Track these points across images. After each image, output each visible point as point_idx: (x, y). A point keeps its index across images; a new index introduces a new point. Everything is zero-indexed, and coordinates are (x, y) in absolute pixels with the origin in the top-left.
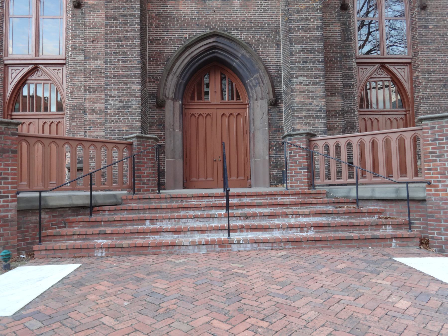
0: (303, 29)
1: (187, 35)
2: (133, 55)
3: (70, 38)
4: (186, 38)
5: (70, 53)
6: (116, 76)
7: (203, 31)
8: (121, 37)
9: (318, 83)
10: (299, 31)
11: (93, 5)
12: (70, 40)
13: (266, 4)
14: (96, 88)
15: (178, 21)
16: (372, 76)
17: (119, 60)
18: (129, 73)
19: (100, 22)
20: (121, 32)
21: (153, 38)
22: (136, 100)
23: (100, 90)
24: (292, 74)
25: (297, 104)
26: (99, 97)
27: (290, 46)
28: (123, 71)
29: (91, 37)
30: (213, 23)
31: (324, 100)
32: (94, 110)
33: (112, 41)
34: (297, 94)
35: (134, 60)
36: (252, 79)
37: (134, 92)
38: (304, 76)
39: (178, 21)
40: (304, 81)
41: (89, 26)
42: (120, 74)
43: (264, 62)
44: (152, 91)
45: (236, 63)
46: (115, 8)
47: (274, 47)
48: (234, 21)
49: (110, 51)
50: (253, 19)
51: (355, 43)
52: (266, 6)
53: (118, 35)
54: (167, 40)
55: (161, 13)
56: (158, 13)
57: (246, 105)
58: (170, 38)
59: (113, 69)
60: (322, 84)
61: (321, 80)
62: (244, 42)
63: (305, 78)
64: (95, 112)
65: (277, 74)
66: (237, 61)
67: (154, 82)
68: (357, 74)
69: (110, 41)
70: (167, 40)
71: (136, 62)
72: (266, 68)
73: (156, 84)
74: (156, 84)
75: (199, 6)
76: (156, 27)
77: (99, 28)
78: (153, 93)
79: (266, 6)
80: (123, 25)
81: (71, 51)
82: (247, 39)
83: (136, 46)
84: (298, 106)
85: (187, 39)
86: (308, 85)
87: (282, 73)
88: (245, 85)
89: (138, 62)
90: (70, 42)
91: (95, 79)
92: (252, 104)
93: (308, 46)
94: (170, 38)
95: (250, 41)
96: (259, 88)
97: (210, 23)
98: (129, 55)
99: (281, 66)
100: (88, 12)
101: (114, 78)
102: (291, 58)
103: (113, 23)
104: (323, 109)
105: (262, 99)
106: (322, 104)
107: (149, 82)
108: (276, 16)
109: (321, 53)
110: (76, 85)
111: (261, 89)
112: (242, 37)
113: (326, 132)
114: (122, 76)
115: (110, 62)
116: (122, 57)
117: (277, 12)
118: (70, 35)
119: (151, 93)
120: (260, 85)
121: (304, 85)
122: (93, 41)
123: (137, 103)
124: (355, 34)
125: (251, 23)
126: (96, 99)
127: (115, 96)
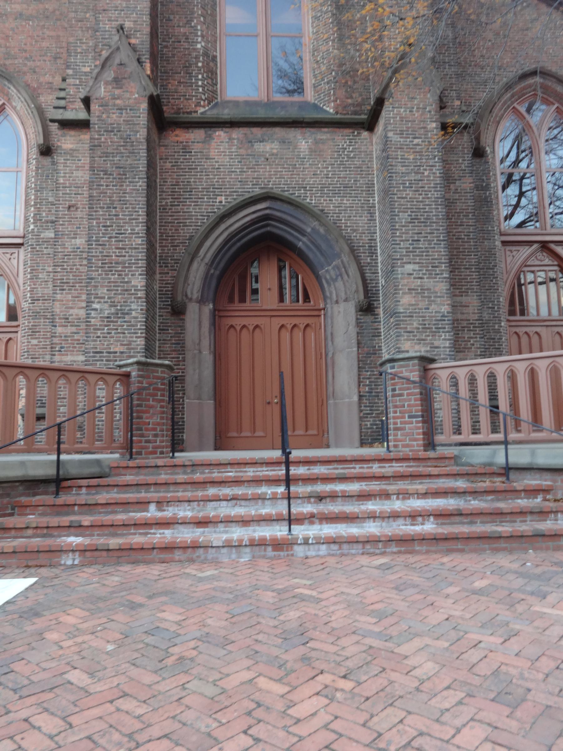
2: (134, 230)
3: (33, 203)
4: (221, 202)
5: (32, 227)
6: (106, 263)
7: (249, 192)
8: (114, 201)
11: (71, 150)
12: (31, 206)
16: (528, 263)
17: (110, 237)
18: (127, 258)
19: (82, 177)
20: (115, 193)
21: (167, 203)
22: (138, 302)
23: (79, 286)
24: (395, 259)
25: (404, 309)
28: (117, 256)
29: (66, 201)
31: (449, 302)
32: (67, 319)
33: (100, 208)
35: (136, 237)
36: (330, 268)
37: (135, 290)
38: (414, 263)
40: (414, 270)
41: (63, 184)
42: (112, 260)
43: (350, 243)
45: (304, 243)
46: (107, 154)
48: (299, 175)
49: (97, 223)
50: (330, 171)
51: (498, 210)
53: (110, 197)
54: (191, 205)
55: (181, 162)
56: (175, 162)
57: (320, 310)
59: (101, 252)
60: (444, 275)
62: (315, 209)
63: (416, 267)
64: (69, 322)
66: (304, 239)
68: (503, 260)
69: (97, 208)
71: (139, 241)
72: (353, 251)
75: (243, 151)
76: (172, 185)
77: (79, 187)
80: (118, 182)
81: (33, 223)
82: (321, 203)
83: (139, 215)
84: (406, 313)
85: (223, 203)
86: (421, 278)
88: (318, 278)
89: (142, 241)
90: (32, 209)
92: (329, 309)
95: (326, 207)
96: (342, 283)
98: (127, 230)
100: (63, 161)
102: (392, 233)
104: (446, 317)
105: (346, 300)
106: (445, 309)
107: (160, 273)
109: (442, 226)
111: (344, 283)
114: (117, 263)
115: (96, 241)
116: (116, 234)
120: (342, 278)
121: (415, 278)
122: (69, 207)
123: (139, 308)
124: (497, 195)
126: (71, 301)
127: (103, 295)
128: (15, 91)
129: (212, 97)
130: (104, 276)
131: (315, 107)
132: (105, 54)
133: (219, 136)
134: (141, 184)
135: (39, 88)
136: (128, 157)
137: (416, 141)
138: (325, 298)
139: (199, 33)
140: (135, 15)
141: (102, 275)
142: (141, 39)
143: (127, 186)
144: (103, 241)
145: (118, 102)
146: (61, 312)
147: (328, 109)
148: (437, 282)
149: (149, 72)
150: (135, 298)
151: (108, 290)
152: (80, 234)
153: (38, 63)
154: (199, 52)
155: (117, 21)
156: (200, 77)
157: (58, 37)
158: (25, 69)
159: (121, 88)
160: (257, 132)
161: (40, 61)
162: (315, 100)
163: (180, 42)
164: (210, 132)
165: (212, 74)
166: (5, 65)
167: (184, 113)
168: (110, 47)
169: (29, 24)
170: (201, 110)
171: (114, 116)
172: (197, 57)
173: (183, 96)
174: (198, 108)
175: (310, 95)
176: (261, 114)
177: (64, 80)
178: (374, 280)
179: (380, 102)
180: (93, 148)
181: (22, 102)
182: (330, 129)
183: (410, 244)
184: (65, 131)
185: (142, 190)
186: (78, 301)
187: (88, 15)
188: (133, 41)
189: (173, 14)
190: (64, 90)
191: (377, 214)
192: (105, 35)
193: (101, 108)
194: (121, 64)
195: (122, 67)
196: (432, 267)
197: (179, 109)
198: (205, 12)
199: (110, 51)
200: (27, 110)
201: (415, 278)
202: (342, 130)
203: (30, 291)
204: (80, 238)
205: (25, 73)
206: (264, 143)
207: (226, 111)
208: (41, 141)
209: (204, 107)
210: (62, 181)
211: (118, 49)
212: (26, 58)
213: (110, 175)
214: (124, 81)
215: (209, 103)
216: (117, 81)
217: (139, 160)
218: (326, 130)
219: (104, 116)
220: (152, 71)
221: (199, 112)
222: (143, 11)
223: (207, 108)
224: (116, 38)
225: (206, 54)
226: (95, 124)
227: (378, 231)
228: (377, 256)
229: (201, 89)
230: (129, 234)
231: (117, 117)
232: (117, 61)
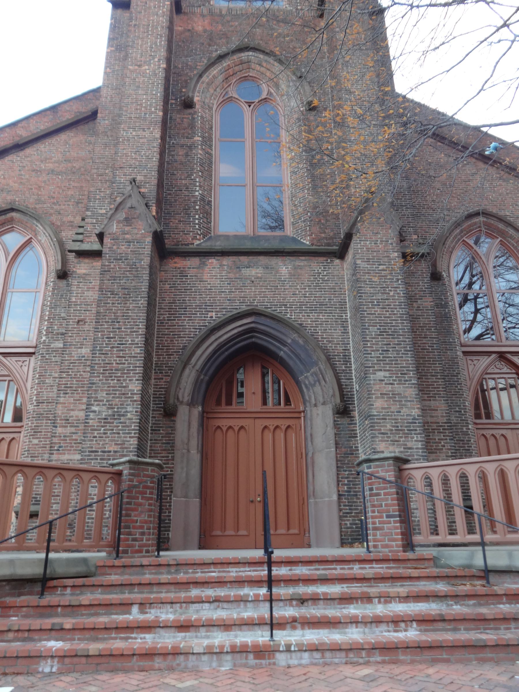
0: (379, 305)
1: (214, 313)
2: (134, 341)
3: (47, 318)
5: (44, 338)
6: (107, 370)
7: (237, 309)
8: (118, 316)
9: (407, 381)
10: (374, 308)
11: (84, 274)
12: (45, 321)
14: (76, 387)
16: (489, 371)
17: (113, 347)
18: (126, 365)
19: (91, 296)
21: (164, 318)
22: (133, 405)
23: (81, 390)
24: (367, 367)
25: (377, 412)
26: (79, 400)
27: (363, 329)
28: (117, 364)
29: (76, 316)
30: (251, 297)
31: (419, 406)
32: (68, 420)
33: (106, 322)
34: (376, 398)
35: (135, 347)
36: (309, 374)
37: (131, 394)
38: (385, 370)
40: (385, 377)
41: (75, 302)
42: (113, 367)
44: (158, 391)
45: (284, 352)
46: (114, 278)
47: (339, 330)
50: (307, 292)
51: (457, 324)
54: (185, 320)
59: (103, 360)
60: (413, 382)
61: (411, 377)
62: (295, 323)
63: (387, 374)
64: (69, 423)
65: (345, 367)
66: (285, 349)
67: (162, 379)
70: (185, 320)
71: (138, 350)
72: (329, 359)
73: (165, 382)
74: (165, 382)
75: (231, 275)
77: (88, 305)
78: (160, 394)
81: (46, 335)
83: (139, 328)
84: (379, 415)
85: (214, 318)
86: (392, 384)
87: (353, 365)
88: (298, 383)
89: (141, 350)
90: (46, 323)
91: (75, 375)
92: (309, 412)
93: (389, 329)
96: (319, 388)
98: (128, 341)
99: (350, 355)
101: (103, 374)
103: (110, 297)
104: (417, 419)
105: (324, 404)
106: (416, 412)
107: (155, 379)
109: (408, 338)
110: (46, 383)
112: (292, 316)
114: (116, 370)
115: (99, 350)
116: (118, 344)
118: (47, 313)
119: (156, 394)
120: (320, 383)
121: (386, 384)
122: (79, 321)
123: (134, 410)
126: (73, 403)
127: (102, 399)
129: (206, 232)
130: (104, 381)
131: (294, 240)
132: (119, 200)
133: (212, 263)
134: (143, 302)
135: (61, 225)
136: (133, 280)
137: (381, 267)
138: (304, 402)
139: (198, 184)
141: (102, 380)
142: (150, 188)
143: (130, 304)
144: (106, 350)
145: (127, 236)
146: (63, 413)
147: (305, 241)
148: (407, 387)
149: (154, 214)
150: (131, 401)
151: (107, 394)
152: (86, 345)
153: (63, 207)
156: (197, 217)
157: (82, 187)
158: (52, 211)
159: (131, 226)
160: (244, 259)
164: (204, 260)
165: (207, 215)
166: (35, 208)
167: (182, 245)
169: (58, 178)
170: (198, 242)
171: (123, 247)
172: (195, 202)
174: (194, 241)
175: (289, 231)
176: (248, 245)
177: (83, 219)
178: (349, 385)
179: (349, 237)
180: (103, 273)
181: (46, 236)
182: (307, 258)
183: (380, 354)
184: (81, 259)
185: (143, 307)
186: (79, 403)
187: (107, 171)
188: (142, 190)
190: (83, 227)
191: (350, 328)
194: (132, 208)
195: (133, 210)
196: (401, 374)
197: (178, 242)
198: (203, 169)
199: (123, 197)
201: (386, 384)
202: (317, 258)
203: (36, 395)
204: (86, 348)
205: (51, 215)
207: (218, 243)
208: (59, 267)
209: (199, 240)
210: (74, 300)
211: (130, 196)
212: (54, 203)
213: (116, 294)
214: (133, 220)
216: (128, 221)
217: (142, 282)
218: (303, 258)
220: (157, 212)
223: (202, 241)
224: (129, 188)
225: (202, 199)
226: (107, 254)
227: (351, 342)
228: (351, 364)
229: (197, 226)
230: (130, 344)
232: (129, 205)
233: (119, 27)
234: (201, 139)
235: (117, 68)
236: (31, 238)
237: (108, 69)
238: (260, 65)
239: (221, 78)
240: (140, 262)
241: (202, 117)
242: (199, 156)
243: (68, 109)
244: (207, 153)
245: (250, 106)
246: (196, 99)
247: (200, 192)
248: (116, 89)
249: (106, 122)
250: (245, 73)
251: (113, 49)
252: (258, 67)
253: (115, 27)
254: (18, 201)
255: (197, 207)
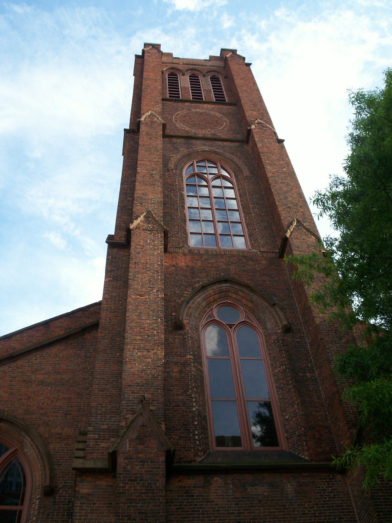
11: (88, 494)
13: (330, 489)
15: (210, 517)
19: (96, 519)
39: (210, 517)
48: (290, 514)
52: (330, 492)
55: (185, 505)
56: (180, 505)
58: (194, 511)
79: (330, 492)
94: (194, 511)
97: (257, 519)
100: (79, 504)
108: (348, 506)
113: (88, 447)
117: (347, 500)
125: (315, 517)
128: (29, 440)
132: (130, 417)
133: (217, 481)
139: (194, 400)
140: (152, 389)
145: (141, 455)
147: (303, 457)
154: (195, 414)
155: (139, 393)
156: (196, 432)
159: (143, 445)
161: (53, 416)
162: (290, 449)
163: (179, 406)
168: (134, 412)
169: (48, 389)
170: (200, 459)
171: (138, 467)
172: (193, 418)
173: (184, 448)
174: (196, 458)
175: (284, 445)
181: (34, 449)
188: (151, 408)
189: (172, 386)
192: (129, 403)
193: (126, 461)
194: (143, 426)
198: (197, 385)
199: (135, 416)
200: (37, 455)
206: (256, 487)
208: (48, 483)
209: (201, 456)
212: (42, 414)
213: (134, 520)
215: (204, 453)
216: (141, 439)
218: (306, 474)
219: (129, 467)
221: (197, 461)
222: (158, 386)
223: (203, 457)
225: (199, 415)
226: (121, 474)
229: (198, 442)
231: (140, 468)
233: (115, 262)
234: (192, 357)
235: (114, 294)
236: (16, 450)
237: (107, 295)
238: (236, 294)
239: (204, 304)
240: (156, 484)
241: (192, 338)
242: (193, 373)
243: (59, 325)
244: (199, 369)
245: (231, 328)
246: (185, 322)
247: (197, 407)
248: (114, 312)
249: (106, 341)
250: (223, 300)
251: (110, 279)
252: (235, 296)
253: (112, 261)
254: (8, 412)
255: (196, 423)
